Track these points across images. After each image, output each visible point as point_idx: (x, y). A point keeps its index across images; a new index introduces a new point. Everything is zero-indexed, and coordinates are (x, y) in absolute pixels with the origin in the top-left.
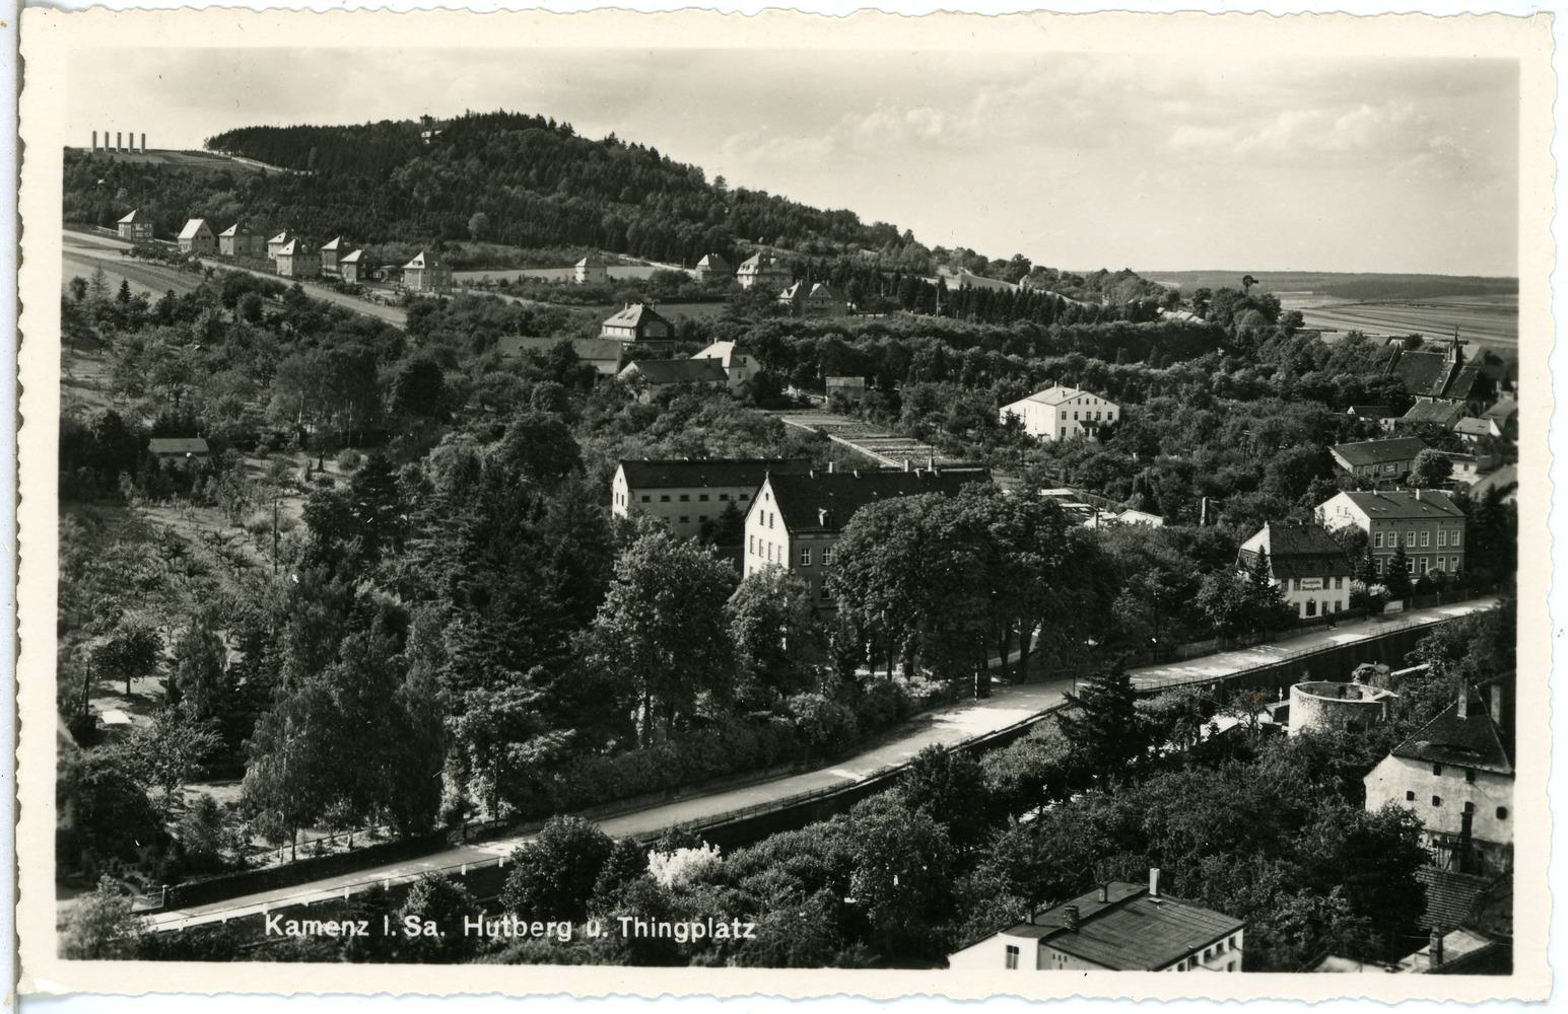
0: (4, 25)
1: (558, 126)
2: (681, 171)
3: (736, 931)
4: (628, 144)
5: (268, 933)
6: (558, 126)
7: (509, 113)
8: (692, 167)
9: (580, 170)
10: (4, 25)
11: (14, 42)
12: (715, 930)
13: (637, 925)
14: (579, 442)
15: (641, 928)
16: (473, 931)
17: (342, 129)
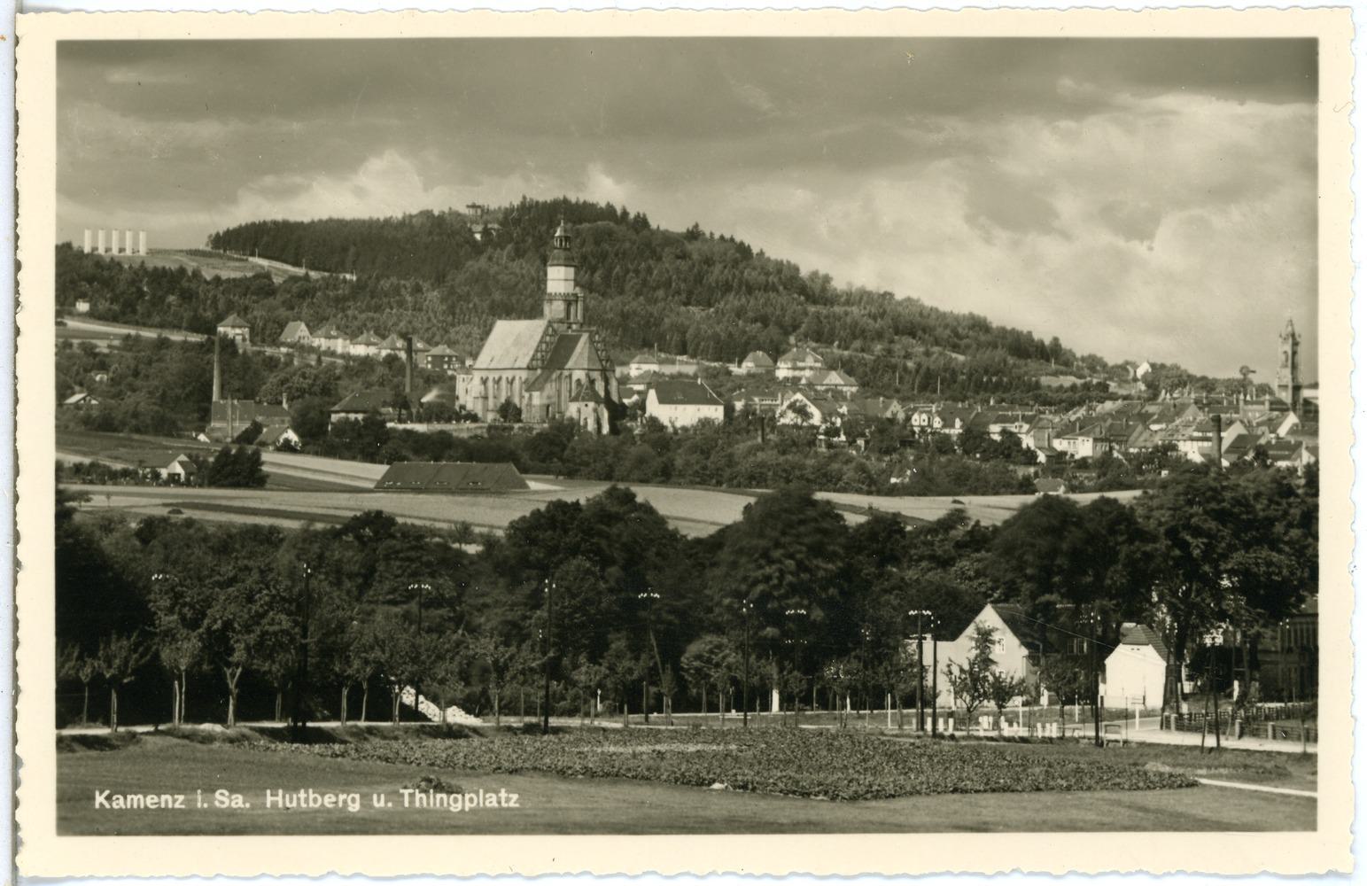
0: (3, 38)
1: (632, 216)
2: (780, 267)
3: (503, 801)
4: (717, 236)
5: (97, 806)
6: (632, 216)
7: (573, 200)
8: (788, 262)
9: (649, 270)
10: (3, 38)
11: (12, 428)
12: (485, 799)
13: (418, 796)
14: (888, 415)
16: (274, 804)
17: (387, 222)
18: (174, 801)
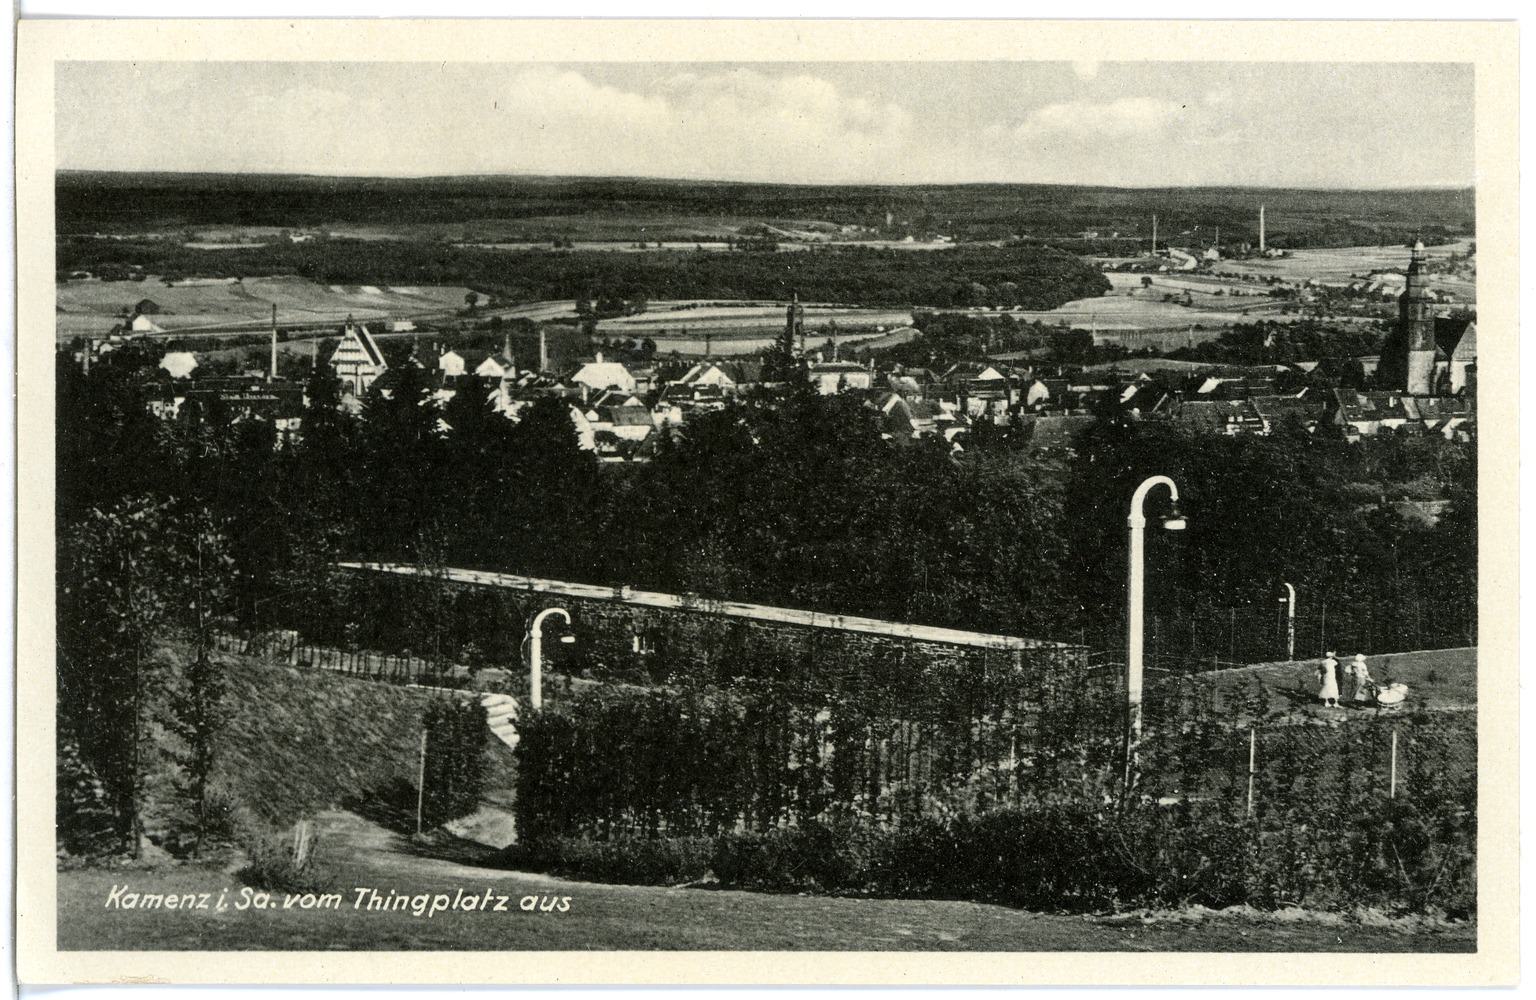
15: (375, 903)
18: (198, 900)
